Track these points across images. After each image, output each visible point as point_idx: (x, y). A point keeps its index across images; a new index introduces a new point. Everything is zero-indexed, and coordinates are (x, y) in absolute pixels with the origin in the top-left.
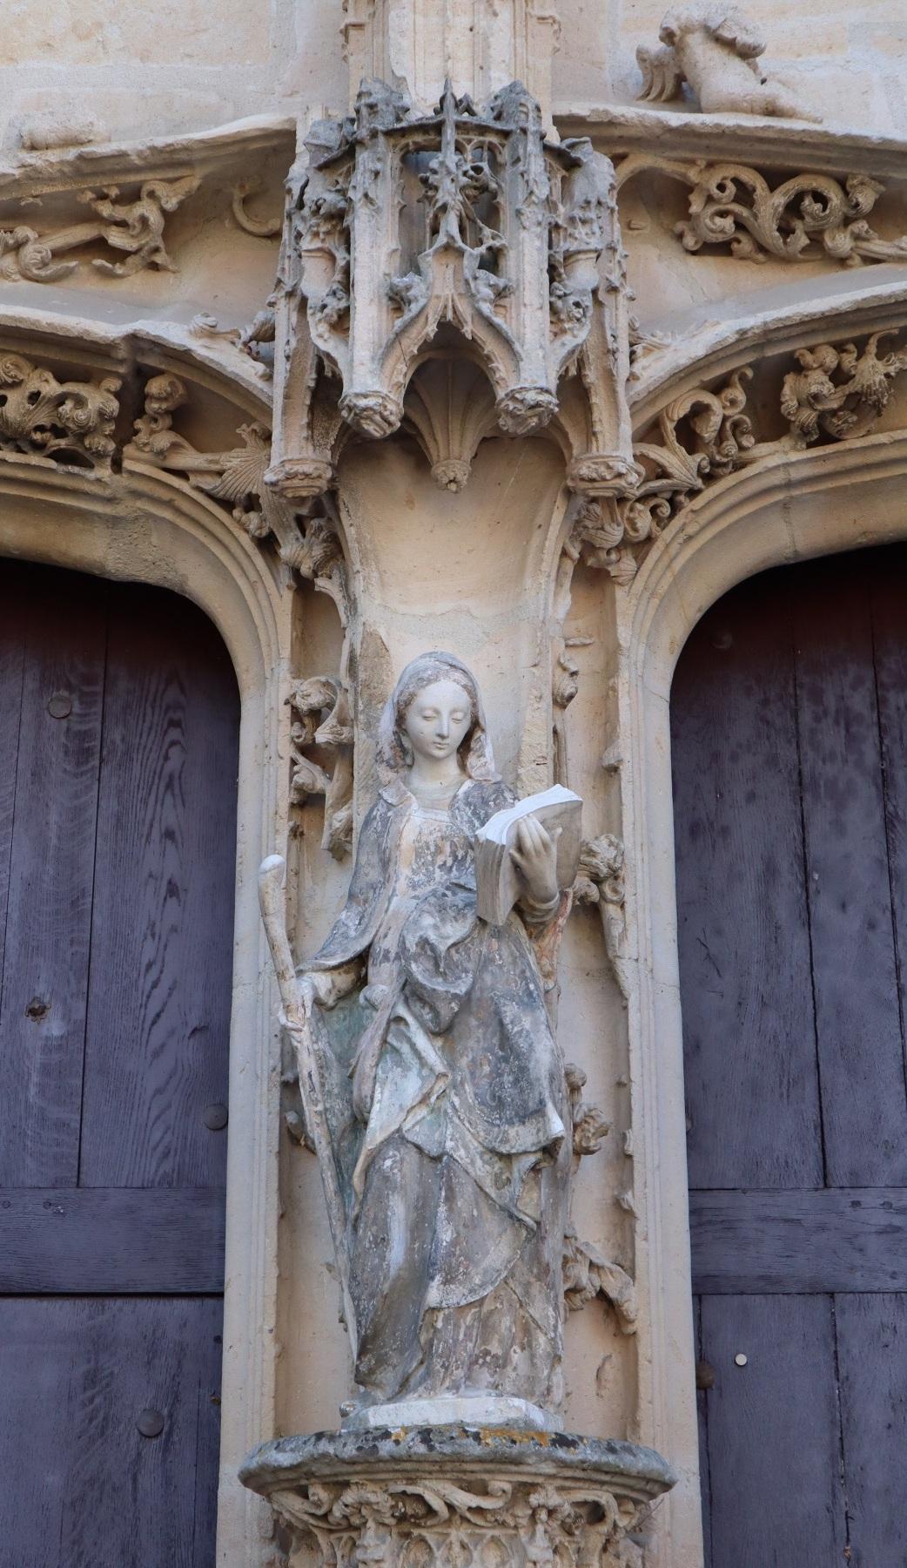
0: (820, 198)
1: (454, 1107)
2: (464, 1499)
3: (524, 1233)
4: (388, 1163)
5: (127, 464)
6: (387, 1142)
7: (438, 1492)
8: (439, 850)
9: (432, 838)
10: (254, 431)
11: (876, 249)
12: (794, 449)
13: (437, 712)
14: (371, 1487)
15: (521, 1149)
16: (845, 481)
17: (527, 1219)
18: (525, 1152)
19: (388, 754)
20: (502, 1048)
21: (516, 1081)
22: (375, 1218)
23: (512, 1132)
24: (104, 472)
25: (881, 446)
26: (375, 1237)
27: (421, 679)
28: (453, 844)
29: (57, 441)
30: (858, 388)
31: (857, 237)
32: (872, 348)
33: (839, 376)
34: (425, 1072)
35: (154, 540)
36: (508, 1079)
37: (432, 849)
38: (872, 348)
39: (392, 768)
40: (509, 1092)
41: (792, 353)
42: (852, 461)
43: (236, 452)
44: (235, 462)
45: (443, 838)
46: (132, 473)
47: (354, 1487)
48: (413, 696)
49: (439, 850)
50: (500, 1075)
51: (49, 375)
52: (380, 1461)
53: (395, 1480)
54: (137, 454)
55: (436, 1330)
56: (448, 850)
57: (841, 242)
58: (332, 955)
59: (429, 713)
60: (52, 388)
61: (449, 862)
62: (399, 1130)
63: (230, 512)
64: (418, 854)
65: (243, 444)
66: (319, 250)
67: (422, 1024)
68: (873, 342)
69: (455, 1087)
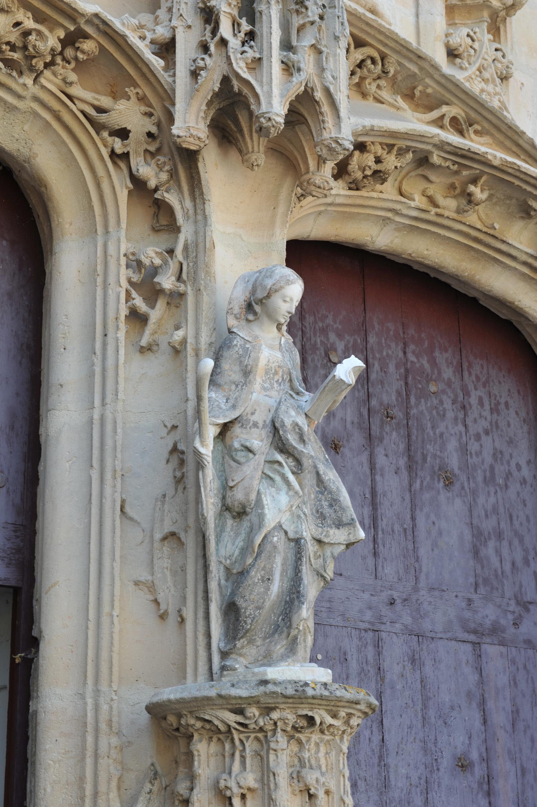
0: (374, 61)
1: (305, 514)
2: (329, 720)
3: (322, 584)
4: (275, 539)
5: (42, 80)
6: (274, 528)
7: (320, 715)
8: (276, 373)
9: (273, 365)
10: (137, 93)
11: (385, 97)
12: (343, 188)
13: (292, 300)
14: (288, 711)
15: (337, 542)
16: (347, 209)
17: (328, 577)
18: (339, 544)
19: (236, 310)
20: (318, 486)
21: (331, 506)
22: (265, 567)
23: (331, 532)
24: (28, 80)
25: (372, 198)
26: (263, 577)
27: (289, 280)
28: (283, 371)
29: (12, 53)
30: (383, 169)
31: (379, 87)
32: (395, 151)
33: (378, 161)
34: (291, 493)
35: (26, 128)
36: (325, 504)
37: (273, 371)
38: (395, 151)
39: (237, 318)
40: (327, 511)
41: (366, 142)
42: (359, 202)
43: (123, 101)
44: (121, 107)
45: (279, 367)
46: (43, 87)
47: (278, 710)
48: (282, 288)
49: (276, 373)
50: (320, 501)
51: (30, 15)
52: (306, 698)
53: (303, 709)
54: (52, 77)
55: (299, 631)
56: (281, 373)
57: (372, 88)
58: (218, 417)
59: (288, 299)
60: (29, 24)
61: (280, 381)
62: (279, 522)
63: (98, 133)
64: (267, 373)
65: (129, 98)
66: (230, 14)
67: (289, 467)
68: (396, 148)
69: (305, 504)
